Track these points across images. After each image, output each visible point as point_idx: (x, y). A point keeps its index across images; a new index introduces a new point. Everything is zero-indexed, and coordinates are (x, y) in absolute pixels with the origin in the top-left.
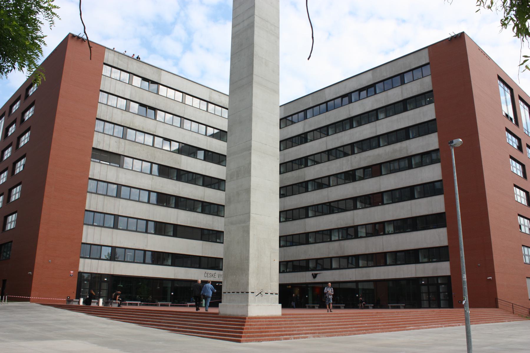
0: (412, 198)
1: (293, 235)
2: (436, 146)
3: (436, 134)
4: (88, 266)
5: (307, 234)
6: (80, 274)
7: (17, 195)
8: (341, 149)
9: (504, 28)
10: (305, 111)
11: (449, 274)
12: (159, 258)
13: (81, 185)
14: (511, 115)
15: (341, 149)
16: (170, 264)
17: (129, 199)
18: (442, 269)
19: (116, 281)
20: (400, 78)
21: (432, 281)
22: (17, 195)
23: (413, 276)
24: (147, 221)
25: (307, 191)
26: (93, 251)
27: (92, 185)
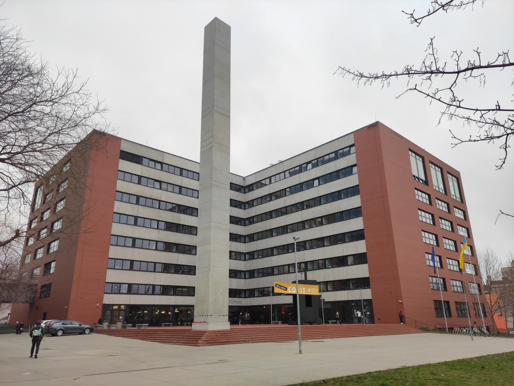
0: (344, 241)
1: (263, 269)
2: (359, 204)
3: (359, 196)
4: (109, 299)
5: (273, 268)
6: (105, 305)
7: (55, 248)
8: (280, 210)
9: (472, 62)
10: (270, 178)
11: (370, 298)
12: (166, 290)
13: (109, 239)
14: (422, 177)
15: (280, 210)
16: (172, 294)
17: (142, 248)
18: (365, 294)
19: (132, 308)
20: (338, 155)
21: (357, 304)
22: (55, 248)
23: (346, 299)
24: (155, 263)
25: (272, 236)
26: (116, 288)
27: (114, 240)
